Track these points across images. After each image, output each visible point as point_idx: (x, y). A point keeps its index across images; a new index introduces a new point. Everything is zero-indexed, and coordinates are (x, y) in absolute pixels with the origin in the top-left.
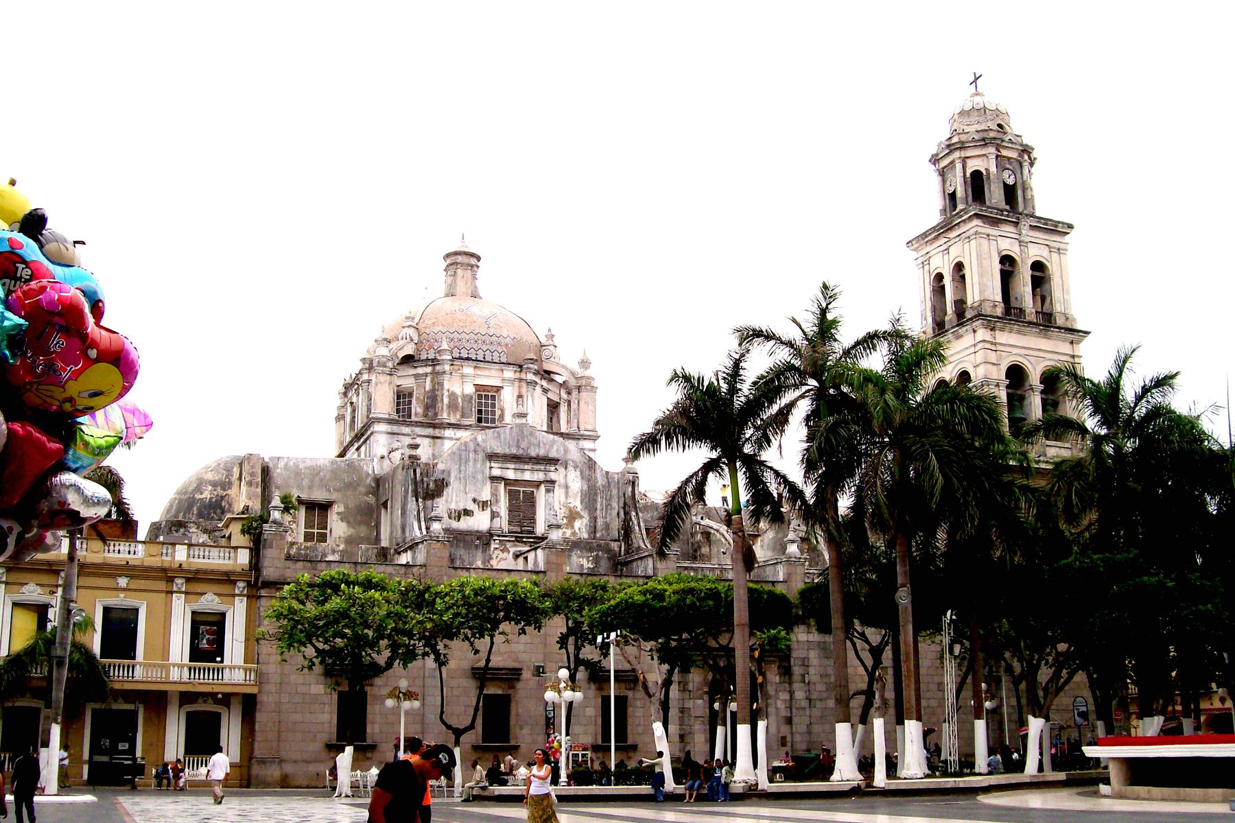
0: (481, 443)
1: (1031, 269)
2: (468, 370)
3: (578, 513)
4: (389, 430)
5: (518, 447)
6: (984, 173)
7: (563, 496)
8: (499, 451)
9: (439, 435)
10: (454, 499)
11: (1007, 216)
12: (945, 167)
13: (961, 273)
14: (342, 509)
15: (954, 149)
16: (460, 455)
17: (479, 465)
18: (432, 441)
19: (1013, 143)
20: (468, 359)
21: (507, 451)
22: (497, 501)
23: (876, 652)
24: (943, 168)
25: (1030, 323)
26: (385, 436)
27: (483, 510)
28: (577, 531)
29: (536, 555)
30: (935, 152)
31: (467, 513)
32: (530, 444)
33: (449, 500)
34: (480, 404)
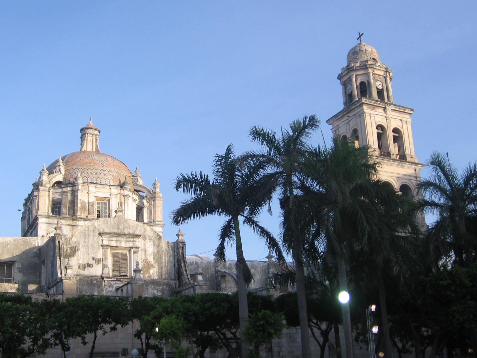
0: (97, 227)
1: (393, 131)
2: (92, 188)
3: (152, 265)
4: (47, 222)
5: (118, 228)
6: (367, 82)
7: (143, 255)
8: (107, 230)
9: (75, 224)
10: (81, 258)
11: (380, 104)
12: (346, 80)
13: (356, 135)
14: (20, 266)
15: (351, 71)
16: (85, 233)
17: (95, 239)
18: (71, 227)
19: (380, 67)
20: (92, 183)
21: (112, 231)
22: (106, 259)
23: (325, 334)
24: (345, 81)
25: (394, 160)
26: (45, 225)
27: (98, 264)
28: (151, 274)
29: (127, 288)
30: (340, 73)
31: (89, 265)
32: (124, 226)
33: (79, 258)
34: (98, 207)
